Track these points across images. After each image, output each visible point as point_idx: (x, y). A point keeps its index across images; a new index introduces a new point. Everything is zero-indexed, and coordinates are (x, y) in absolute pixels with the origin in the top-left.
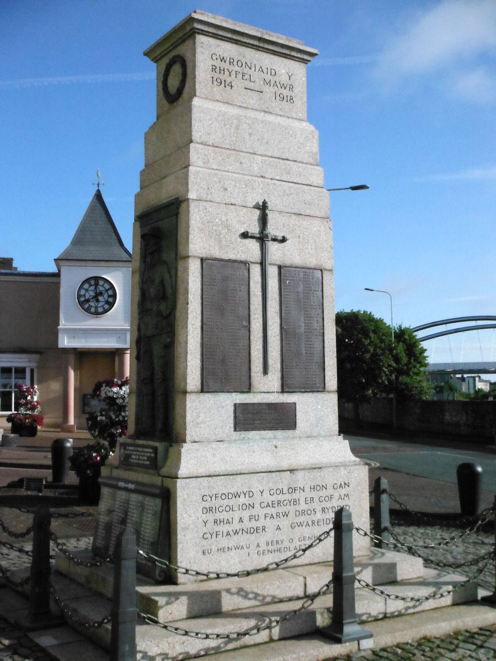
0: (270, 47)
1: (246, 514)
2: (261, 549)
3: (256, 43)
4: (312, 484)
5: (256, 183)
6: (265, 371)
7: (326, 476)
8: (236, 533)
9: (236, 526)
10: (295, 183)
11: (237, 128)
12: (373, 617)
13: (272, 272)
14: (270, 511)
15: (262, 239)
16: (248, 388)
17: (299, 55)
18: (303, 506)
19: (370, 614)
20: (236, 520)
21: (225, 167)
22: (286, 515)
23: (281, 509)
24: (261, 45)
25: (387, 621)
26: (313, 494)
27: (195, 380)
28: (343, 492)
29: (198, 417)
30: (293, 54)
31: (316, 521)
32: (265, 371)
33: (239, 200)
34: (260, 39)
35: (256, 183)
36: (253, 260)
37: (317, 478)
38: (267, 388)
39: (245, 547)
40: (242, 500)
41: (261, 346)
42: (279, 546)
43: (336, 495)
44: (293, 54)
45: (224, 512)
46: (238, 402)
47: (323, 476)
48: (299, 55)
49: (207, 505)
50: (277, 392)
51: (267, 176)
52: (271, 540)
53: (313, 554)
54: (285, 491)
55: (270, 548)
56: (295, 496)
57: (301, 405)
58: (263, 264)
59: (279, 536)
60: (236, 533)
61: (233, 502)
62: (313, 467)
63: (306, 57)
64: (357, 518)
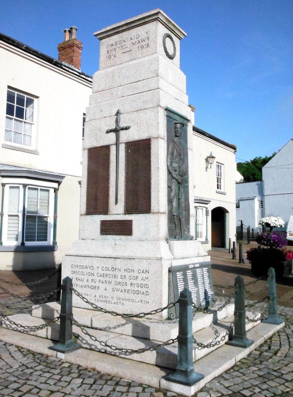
0: (121, 29)
1: (90, 278)
2: (97, 299)
3: (126, 27)
4: (125, 268)
5: (117, 102)
6: (116, 202)
7: (134, 264)
8: (85, 286)
9: (85, 283)
10: (141, 93)
11: (113, 76)
12: (98, 349)
13: (122, 147)
14: (101, 278)
15: (116, 131)
16: (106, 212)
17: (150, 19)
18: (119, 280)
19: (96, 346)
20: (85, 280)
21: (105, 99)
22: (110, 282)
23: (107, 279)
24: (129, 26)
25: (105, 354)
26: (125, 274)
27: (83, 209)
28: (145, 275)
29: (84, 227)
30: (147, 20)
31: (127, 290)
32: (116, 202)
33: (108, 114)
34: (126, 24)
35: (117, 102)
36: (112, 143)
37: (130, 264)
38: (117, 211)
39: (89, 295)
40: (88, 270)
41: (115, 189)
42: (106, 299)
43: (140, 276)
44: (147, 20)
45: (80, 275)
46: (103, 219)
47: (132, 264)
48: (150, 19)
49: (73, 270)
50: (122, 214)
51: (125, 95)
52: (102, 295)
53: (124, 309)
54: (95, 274)
55: (101, 299)
56: (116, 273)
57: (136, 221)
58: (117, 144)
59: (105, 293)
60: (85, 286)
61: (84, 270)
62: (130, 258)
63: (154, 17)
64: (153, 294)
